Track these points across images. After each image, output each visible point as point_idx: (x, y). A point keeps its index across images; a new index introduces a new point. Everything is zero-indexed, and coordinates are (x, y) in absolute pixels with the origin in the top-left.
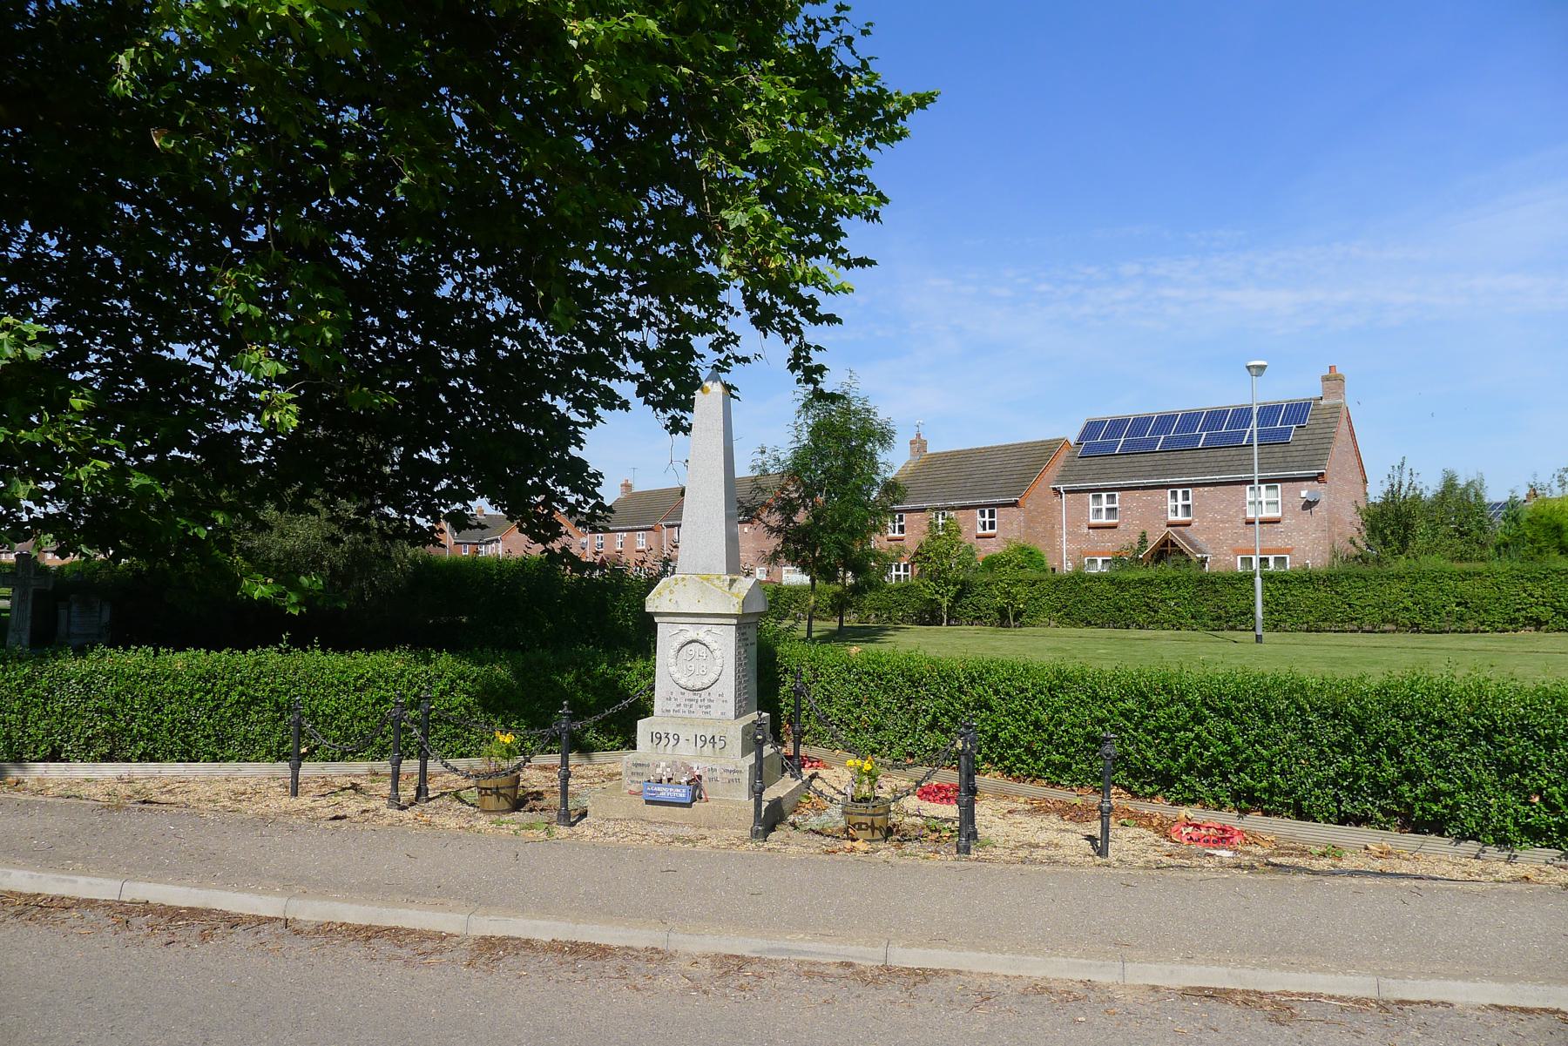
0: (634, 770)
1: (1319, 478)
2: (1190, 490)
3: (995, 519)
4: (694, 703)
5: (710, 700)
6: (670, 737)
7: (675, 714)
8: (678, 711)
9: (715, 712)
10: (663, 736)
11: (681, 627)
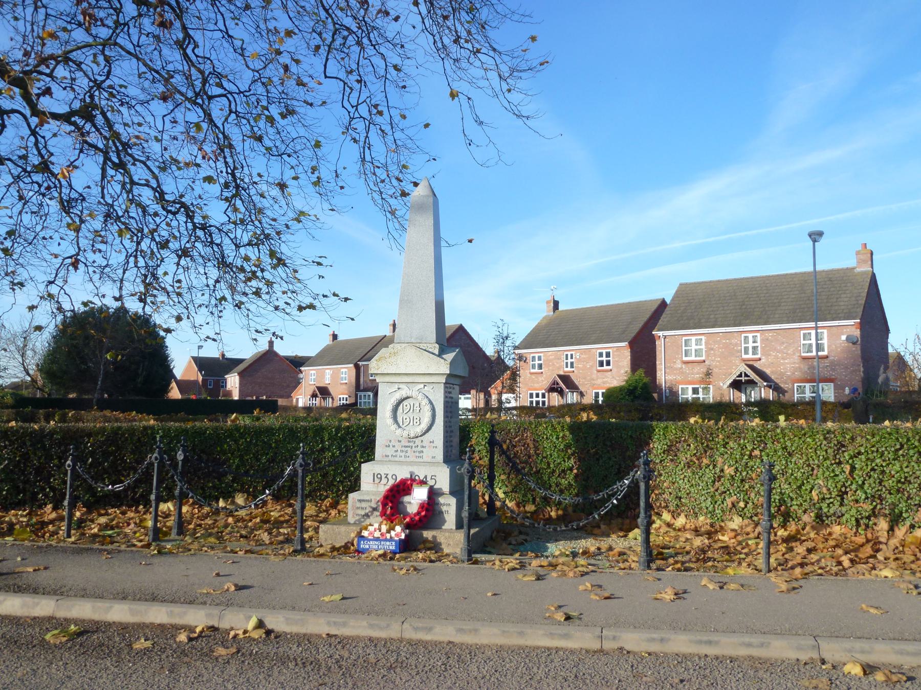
0: (358, 505)
1: (804, 358)
2: (758, 335)
3: (611, 359)
6: (390, 477)
9: (428, 454)
10: (383, 476)
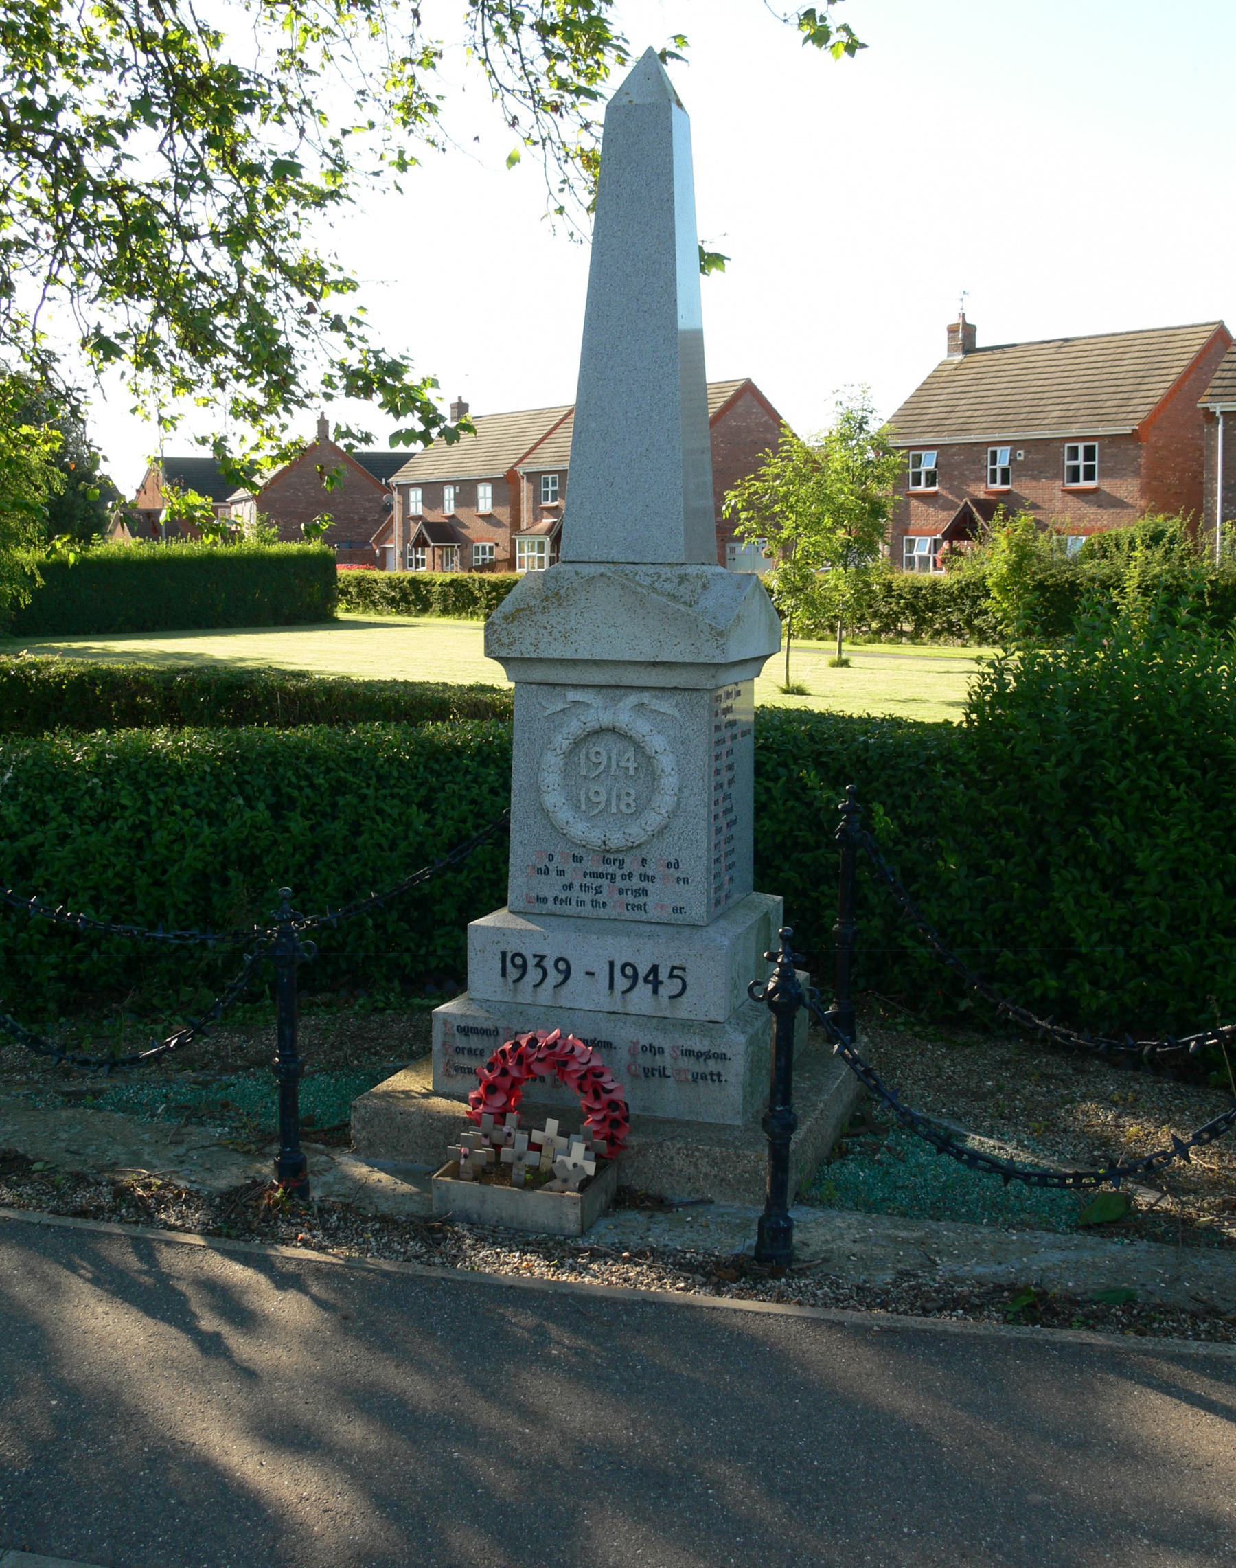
0: (461, 1041)
4: (605, 882)
5: (645, 877)
6: (549, 964)
7: (558, 909)
8: (567, 901)
10: (531, 962)
11: (572, 695)
